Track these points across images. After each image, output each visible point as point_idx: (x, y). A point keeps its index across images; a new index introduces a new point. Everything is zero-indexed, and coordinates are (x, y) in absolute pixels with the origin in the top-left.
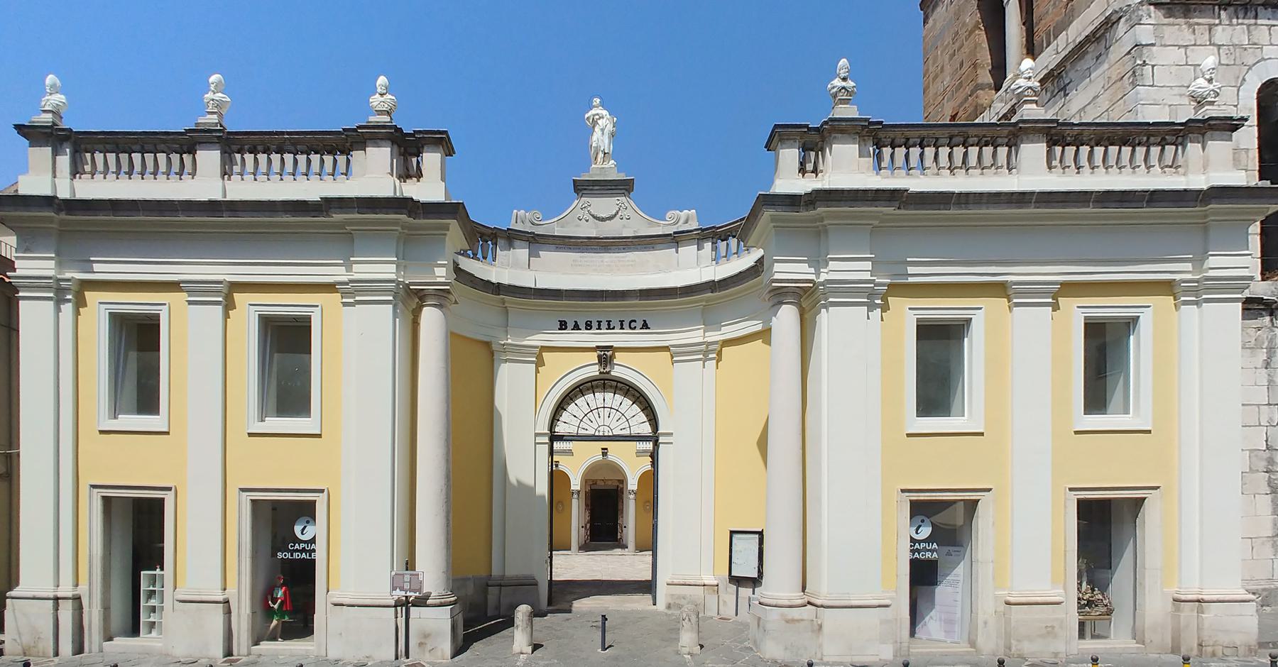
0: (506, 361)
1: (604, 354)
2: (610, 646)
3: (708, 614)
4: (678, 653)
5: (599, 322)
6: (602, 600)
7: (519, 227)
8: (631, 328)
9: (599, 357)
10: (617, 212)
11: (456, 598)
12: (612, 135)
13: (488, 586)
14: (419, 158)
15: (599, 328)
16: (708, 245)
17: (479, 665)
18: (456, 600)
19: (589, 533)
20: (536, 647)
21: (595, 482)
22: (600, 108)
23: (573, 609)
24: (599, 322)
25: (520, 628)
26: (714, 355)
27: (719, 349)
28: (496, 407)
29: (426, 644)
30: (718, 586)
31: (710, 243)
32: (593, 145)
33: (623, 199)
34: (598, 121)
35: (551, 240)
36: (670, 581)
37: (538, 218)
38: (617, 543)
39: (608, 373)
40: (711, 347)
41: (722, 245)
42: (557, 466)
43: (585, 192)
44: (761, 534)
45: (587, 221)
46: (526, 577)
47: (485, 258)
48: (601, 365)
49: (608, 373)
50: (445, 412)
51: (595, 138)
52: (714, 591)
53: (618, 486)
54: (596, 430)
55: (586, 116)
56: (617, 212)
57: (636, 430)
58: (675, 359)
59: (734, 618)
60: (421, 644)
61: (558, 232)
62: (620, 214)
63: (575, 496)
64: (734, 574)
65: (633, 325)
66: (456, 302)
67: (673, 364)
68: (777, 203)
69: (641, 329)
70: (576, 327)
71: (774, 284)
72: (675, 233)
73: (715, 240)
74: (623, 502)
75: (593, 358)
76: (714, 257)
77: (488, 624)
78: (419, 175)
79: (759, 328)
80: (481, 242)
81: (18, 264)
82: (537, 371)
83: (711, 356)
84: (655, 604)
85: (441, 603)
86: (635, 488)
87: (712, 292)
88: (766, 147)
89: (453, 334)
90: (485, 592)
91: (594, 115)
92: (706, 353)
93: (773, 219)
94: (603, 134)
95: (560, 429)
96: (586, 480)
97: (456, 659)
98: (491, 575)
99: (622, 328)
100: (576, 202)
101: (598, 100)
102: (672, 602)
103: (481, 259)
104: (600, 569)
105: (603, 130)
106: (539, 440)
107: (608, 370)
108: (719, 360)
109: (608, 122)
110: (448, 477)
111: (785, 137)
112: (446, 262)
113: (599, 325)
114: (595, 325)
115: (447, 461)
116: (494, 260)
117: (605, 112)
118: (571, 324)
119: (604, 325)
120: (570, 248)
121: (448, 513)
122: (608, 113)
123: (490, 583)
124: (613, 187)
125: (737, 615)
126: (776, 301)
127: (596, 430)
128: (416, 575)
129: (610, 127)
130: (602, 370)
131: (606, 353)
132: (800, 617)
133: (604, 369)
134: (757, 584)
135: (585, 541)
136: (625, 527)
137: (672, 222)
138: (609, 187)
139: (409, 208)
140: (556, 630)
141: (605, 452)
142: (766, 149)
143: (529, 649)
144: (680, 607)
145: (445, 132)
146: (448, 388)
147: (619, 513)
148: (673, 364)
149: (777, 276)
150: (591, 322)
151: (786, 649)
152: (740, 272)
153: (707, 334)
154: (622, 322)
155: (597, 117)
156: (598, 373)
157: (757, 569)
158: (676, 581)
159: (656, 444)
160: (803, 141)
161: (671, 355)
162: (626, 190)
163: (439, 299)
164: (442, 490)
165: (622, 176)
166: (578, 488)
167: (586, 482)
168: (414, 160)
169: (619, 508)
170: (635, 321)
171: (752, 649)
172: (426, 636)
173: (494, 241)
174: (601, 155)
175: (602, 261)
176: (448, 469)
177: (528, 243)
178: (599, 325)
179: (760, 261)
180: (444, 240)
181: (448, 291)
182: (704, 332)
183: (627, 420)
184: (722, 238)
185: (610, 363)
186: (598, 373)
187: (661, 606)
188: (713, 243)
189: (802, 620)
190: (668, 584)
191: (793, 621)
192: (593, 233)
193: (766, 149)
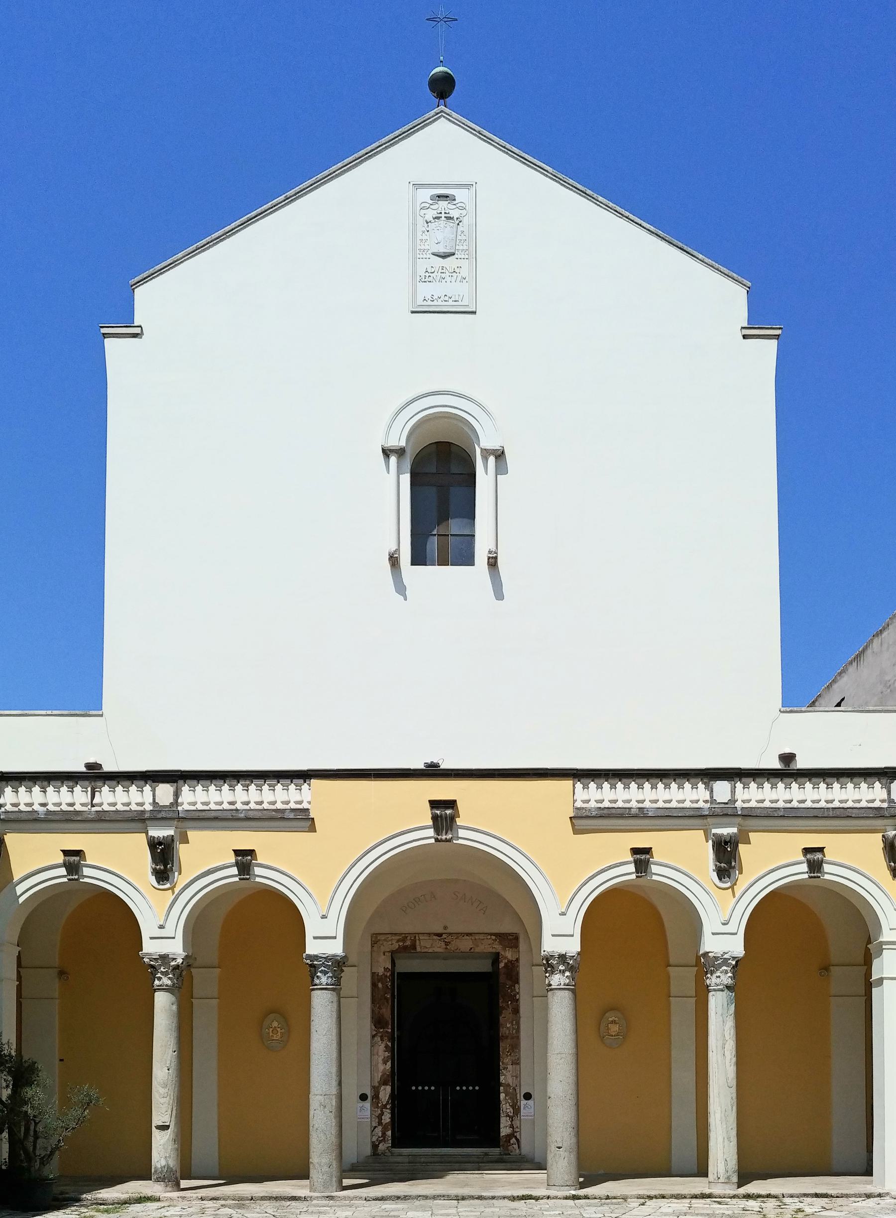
19: (387, 1118)
38: (497, 1151)
53: (496, 958)
74: (516, 1011)
81: (238, 880)
86: (573, 946)
135: (375, 1146)
166: (336, 948)
169: (503, 1031)
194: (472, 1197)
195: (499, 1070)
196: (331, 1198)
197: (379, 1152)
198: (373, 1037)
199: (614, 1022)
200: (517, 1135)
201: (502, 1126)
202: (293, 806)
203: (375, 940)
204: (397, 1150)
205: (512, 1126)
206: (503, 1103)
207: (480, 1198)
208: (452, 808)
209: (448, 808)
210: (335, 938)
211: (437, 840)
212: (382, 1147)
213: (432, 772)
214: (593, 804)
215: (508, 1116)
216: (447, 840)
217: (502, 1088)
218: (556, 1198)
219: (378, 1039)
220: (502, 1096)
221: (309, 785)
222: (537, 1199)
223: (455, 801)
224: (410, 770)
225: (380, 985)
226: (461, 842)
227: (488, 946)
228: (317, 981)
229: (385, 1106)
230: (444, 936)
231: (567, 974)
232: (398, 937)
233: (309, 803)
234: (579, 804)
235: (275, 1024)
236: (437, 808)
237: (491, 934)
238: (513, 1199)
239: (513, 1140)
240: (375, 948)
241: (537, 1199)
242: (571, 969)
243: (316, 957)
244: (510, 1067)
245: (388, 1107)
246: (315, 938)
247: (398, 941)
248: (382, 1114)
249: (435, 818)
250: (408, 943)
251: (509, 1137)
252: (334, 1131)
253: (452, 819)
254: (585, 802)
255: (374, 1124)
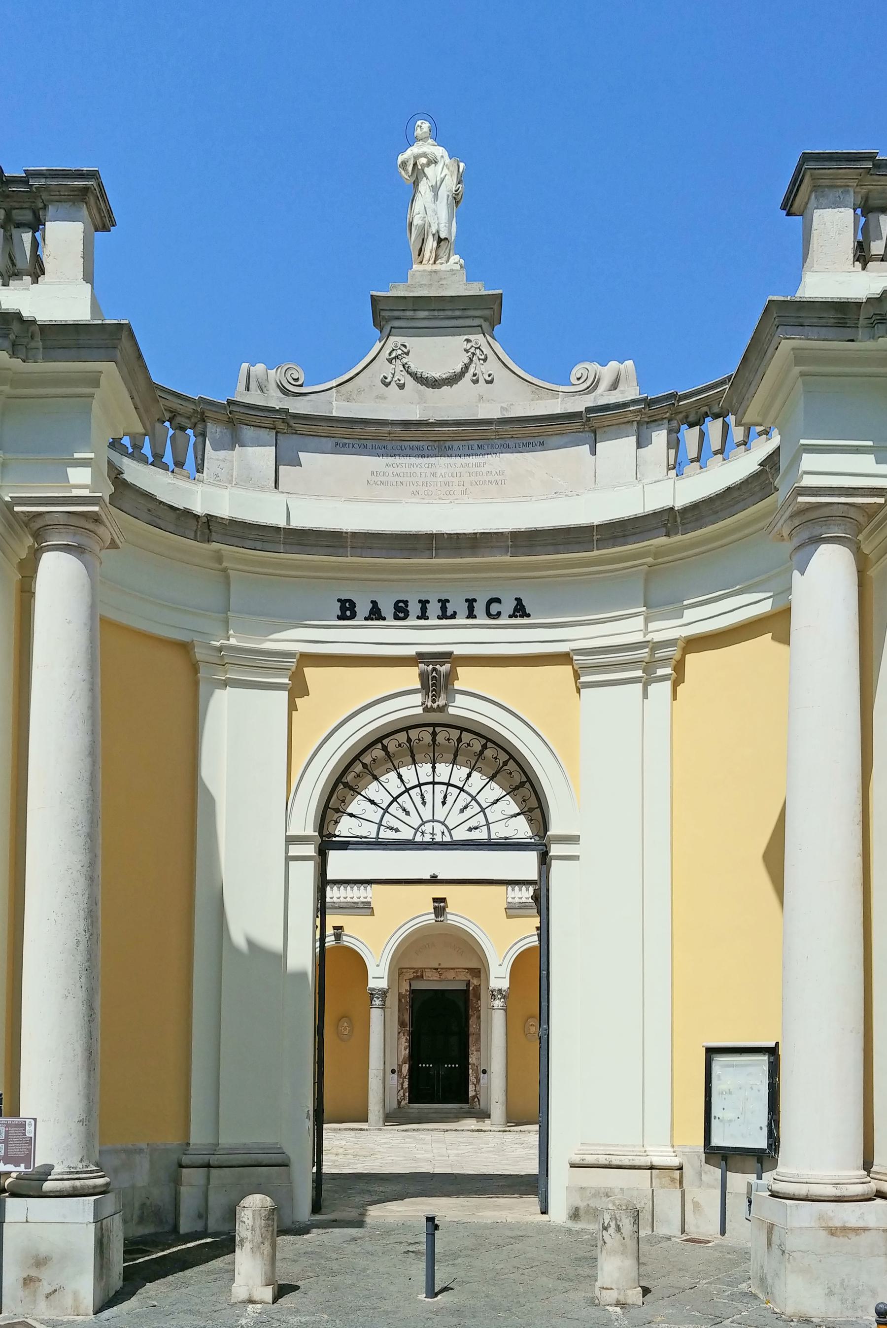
0: (225, 684)
1: (434, 669)
2: (445, 1289)
3: (661, 1230)
4: (593, 1302)
5: (424, 603)
6: (430, 1204)
7: (254, 398)
8: (489, 615)
9: (423, 676)
10: (466, 368)
11: (106, 1180)
12: (456, 200)
13: (181, 1166)
14: (38, 235)
15: (423, 616)
16: (660, 437)
17: (156, 1325)
18: (108, 1184)
19: (406, 1085)
20: (282, 1291)
21: (419, 975)
22: (430, 141)
23: (368, 1220)
24: (424, 603)
25: (248, 1246)
26: (668, 671)
27: (678, 656)
28: (201, 778)
29: (40, 1280)
30: (681, 1169)
31: (665, 432)
32: (415, 223)
33: (479, 339)
34: (426, 170)
35: (323, 428)
36: (577, 1159)
37: (297, 380)
39: (442, 709)
40: (660, 654)
41: (690, 436)
42: (338, 937)
43: (396, 323)
44: (773, 1052)
45: (402, 387)
46: (266, 1150)
47: (179, 464)
48: (427, 694)
49: (442, 709)
50: (87, 775)
51: (418, 206)
52: (673, 1180)
53: (468, 984)
54: (417, 830)
55: (401, 158)
56: (466, 368)
57: (499, 831)
58: (583, 679)
59: (717, 1239)
60: (28, 1281)
61: (339, 408)
62: (472, 370)
63: (377, 1002)
64: (716, 1141)
65: (494, 608)
66: (113, 545)
67: (579, 691)
68: (807, 322)
69: (510, 617)
70: (375, 613)
71: (801, 499)
72: (589, 410)
73: (674, 424)
74: (479, 1017)
75: (410, 677)
76: (672, 462)
77: (179, 1248)
78: (37, 270)
79: (766, 607)
80: (171, 432)
82: (292, 707)
83: (660, 672)
84: (544, 1212)
85: (74, 1188)
86: (505, 984)
87: (668, 535)
88: (783, 208)
89: (105, 622)
90: (176, 1181)
91: (416, 157)
92: (649, 666)
93: (799, 358)
94: (436, 196)
95: (345, 828)
96: (398, 969)
97: (106, 1314)
98: (188, 1144)
99: (471, 615)
100: (378, 346)
101: (426, 126)
102: (582, 1205)
103: (172, 466)
104: (429, 1156)
105: (435, 190)
106: (296, 850)
107: (441, 702)
108: (678, 679)
109: (446, 171)
110: (91, 915)
111: (827, 182)
112: (92, 455)
113: (424, 610)
114: (414, 608)
115: (91, 880)
116: (200, 469)
117: (439, 151)
118: (363, 608)
119: (434, 608)
120: (366, 447)
121: (91, 992)
122: (446, 154)
123: (185, 1160)
124: (458, 313)
125: (723, 1232)
126: (805, 535)
127: (417, 830)
128: (17, 1125)
129: (450, 184)
130: (429, 704)
131: (438, 667)
132: (861, 1224)
133: (434, 701)
134: (766, 1164)
135: (399, 1103)
136: (484, 1072)
137: (585, 386)
138: (449, 313)
139: (12, 337)
140: (328, 1259)
141: (440, 906)
142: (785, 212)
143: (268, 1294)
144: (595, 1213)
145: (94, 175)
146: (93, 724)
147: (471, 1039)
148: (579, 691)
149: (808, 481)
150: (406, 602)
151: (830, 1293)
152: (729, 489)
153: (652, 626)
154: (471, 602)
155: (423, 160)
156: (420, 710)
157: (765, 1130)
158: (590, 1159)
159: (544, 859)
160: (864, 191)
161: (575, 672)
162: (486, 319)
163: (75, 534)
164: (78, 942)
165: (476, 289)
166: (383, 984)
167: (400, 974)
168: (27, 237)
169: (471, 1030)
170: (498, 601)
171: (755, 1297)
172: (40, 1262)
173: (200, 427)
174: (431, 244)
175: (434, 475)
176: (92, 901)
177: (274, 431)
178: (424, 610)
179: (771, 462)
180: (87, 411)
181: (95, 518)
182: (647, 621)
183: (483, 810)
184: (692, 419)
185: (446, 688)
186: (420, 710)
187: (559, 1212)
188: (670, 432)
189: (865, 1229)
190: (573, 1166)
191: (845, 1230)
192: (415, 414)
193: (785, 212)
194: (452, 1130)
195: (469, 1054)
196: (381, 1130)
197: (401, 1106)
198: (399, 1033)
199: (532, 1025)
200: (478, 1096)
201: (470, 1090)
202: (362, 900)
203: (401, 971)
204: (411, 1105)
205: (475, 1091)
206: (471, 1075)
207: (456, 1130)
208: (444, 902)
209: (442, 902)
210: (383, 978)
211: (436, 921)
212: (403, 1103)
213: (434, 880)
214: (517, 900)
215: (473, 1084)
216: (441, 921)
217: (470, 1066)
218: (494, 1131)
219: (401, 1034)
220: (470, 1071)
221: (371, 887)
222: (484, 1131)
223: (445, 898)
224: (422, 879)
225: (403, 1000)
226: (449, 922)
227: (465, 976)
228: (373, 1003)
229: (405, 1077)
230: (439, 970)
231: (502, 1000)
232: (414, 970)
233: (371, 898)
234: (510, 900)
235: (346, 1024)
236: (437, 902)
237: (466, 969)
238: (473, 1131)
239: (476, 1100)
240: (401, 978)
241: (484, 1131)
242: (504, 997)
243: (374, 989)
244: (475, 1053)
245: (407, 1077)
246: (373, 978)
247: (414, 973)
248: (403, 1082)
249: (435, 908)
250: (419, 974)
251: (475, 1096)
252: (381, 1091)
253: (444, 909)
254: (513, 898)
255: (399, 1089)
